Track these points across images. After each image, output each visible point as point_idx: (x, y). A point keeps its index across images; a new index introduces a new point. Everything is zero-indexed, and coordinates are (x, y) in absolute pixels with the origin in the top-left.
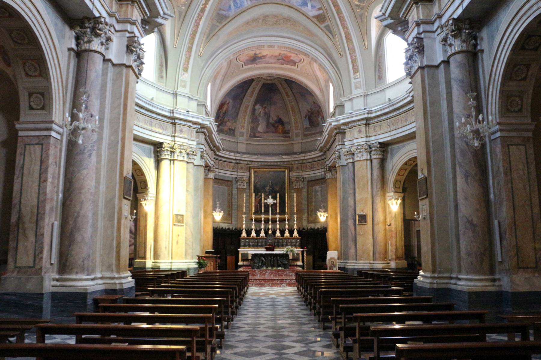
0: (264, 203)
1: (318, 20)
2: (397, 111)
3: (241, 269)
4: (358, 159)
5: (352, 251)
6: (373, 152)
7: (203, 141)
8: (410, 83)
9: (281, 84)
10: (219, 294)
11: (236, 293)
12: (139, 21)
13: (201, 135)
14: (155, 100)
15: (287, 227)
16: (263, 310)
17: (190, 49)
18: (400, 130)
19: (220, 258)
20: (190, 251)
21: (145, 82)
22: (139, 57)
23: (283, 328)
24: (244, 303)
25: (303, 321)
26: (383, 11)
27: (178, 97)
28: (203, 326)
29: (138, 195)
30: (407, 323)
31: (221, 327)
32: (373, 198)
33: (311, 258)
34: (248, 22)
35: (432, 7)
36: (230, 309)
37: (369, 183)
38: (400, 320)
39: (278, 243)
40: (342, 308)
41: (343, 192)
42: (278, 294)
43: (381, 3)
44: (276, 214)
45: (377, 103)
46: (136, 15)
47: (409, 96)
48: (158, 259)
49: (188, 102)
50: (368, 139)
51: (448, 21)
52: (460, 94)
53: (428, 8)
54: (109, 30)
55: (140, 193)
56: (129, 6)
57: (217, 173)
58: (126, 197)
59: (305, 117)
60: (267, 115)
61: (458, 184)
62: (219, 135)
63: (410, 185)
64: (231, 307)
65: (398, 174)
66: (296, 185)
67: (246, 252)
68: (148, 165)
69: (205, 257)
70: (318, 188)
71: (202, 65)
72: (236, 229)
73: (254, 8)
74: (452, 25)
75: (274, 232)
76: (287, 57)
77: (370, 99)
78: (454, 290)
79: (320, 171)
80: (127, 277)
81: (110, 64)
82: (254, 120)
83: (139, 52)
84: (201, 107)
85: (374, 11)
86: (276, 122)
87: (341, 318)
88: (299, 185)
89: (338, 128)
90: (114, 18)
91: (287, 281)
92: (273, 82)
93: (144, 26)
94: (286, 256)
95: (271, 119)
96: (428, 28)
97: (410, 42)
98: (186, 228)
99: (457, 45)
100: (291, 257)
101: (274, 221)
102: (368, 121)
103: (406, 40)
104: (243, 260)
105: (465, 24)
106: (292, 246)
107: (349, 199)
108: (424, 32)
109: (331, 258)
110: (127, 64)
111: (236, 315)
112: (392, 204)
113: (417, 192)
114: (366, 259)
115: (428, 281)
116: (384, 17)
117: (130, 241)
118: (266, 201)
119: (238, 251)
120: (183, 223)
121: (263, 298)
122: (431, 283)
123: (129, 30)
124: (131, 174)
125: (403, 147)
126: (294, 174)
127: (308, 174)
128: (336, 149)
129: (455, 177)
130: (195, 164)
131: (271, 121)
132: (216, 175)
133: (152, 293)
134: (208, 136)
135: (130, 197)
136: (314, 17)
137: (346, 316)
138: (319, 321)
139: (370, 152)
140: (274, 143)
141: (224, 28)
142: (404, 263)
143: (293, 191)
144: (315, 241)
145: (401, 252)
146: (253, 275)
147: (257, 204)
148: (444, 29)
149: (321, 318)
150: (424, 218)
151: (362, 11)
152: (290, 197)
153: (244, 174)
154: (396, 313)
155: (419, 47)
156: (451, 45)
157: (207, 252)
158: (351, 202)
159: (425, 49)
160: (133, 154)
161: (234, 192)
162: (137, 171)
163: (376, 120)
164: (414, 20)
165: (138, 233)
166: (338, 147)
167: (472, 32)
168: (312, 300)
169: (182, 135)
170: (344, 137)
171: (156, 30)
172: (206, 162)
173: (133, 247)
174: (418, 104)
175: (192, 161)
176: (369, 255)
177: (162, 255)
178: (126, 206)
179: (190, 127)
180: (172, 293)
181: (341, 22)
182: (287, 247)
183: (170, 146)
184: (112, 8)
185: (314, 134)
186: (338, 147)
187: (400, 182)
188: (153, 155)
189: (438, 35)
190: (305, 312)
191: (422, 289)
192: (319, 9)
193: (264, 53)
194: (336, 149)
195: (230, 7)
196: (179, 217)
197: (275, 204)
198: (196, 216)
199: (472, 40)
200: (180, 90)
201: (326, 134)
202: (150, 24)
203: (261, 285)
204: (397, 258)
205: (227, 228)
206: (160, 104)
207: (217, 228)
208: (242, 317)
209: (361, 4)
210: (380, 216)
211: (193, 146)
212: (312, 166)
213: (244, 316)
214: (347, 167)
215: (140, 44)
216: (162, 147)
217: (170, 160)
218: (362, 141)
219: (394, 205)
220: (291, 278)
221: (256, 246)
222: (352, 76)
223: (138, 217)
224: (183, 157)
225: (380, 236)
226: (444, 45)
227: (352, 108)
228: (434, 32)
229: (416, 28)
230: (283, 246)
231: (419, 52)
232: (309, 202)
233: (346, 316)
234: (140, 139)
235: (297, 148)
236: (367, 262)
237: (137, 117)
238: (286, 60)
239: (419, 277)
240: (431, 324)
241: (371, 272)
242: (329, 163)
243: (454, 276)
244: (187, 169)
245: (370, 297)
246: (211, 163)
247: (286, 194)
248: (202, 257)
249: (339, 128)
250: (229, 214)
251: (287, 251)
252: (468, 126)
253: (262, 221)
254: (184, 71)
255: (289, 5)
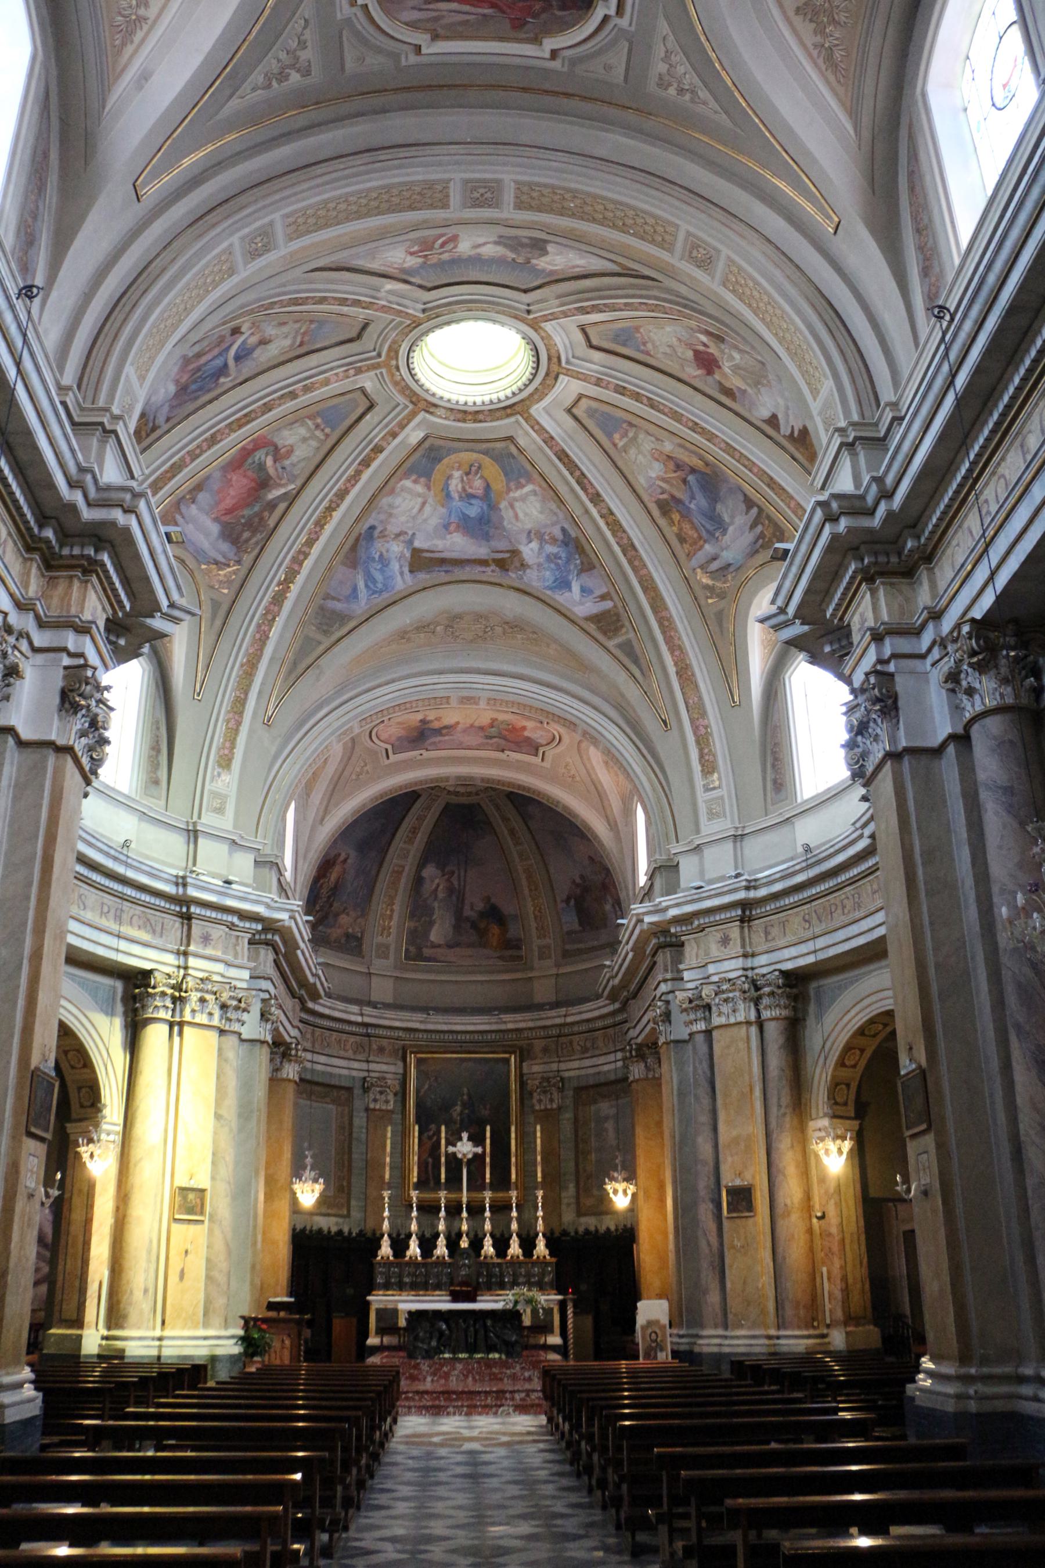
0: (447, 1155)
1: (599, 628)
2: (827, 881)
3: (374, 1360)
4: (723, 1020)
5: (713, 1298)
6: (766, 1001)
7: (270, 970)
8: (865, 799)
9: (498, 807)
10: (302, 1438)
11: (359, 1438)
12: (101, 624)
13: (262, 952)
14: (133, 846)
15: (514, 1226)
16: (441, 1491)
17: (239, 705)
18: (841, 935)
19: (310, 1324)
20: (220, 1302)
21: (110, 795)
22: (95, 725)
23: (505, 1551)
24: (385, 1470)
25: (570, 1526)
26: (780, 602)
27: (201, 841)
28: (255, 1547)
29: (70, 1127)
30: (896, 1530)
31: (309, 1552)
32: (768, 1135)
33: (588, 1321)
34: (406, 632)
35: (914, 590)
36: (339, 1488)
37: (758, 1092)
38: (870, 1519)
39: (490, 1275)
40: (689, 1481)
41: (680, 1121)
42: (488, 1439)
43: (772, 581)
44: (482, 1188)
45: (771, 860)
46: (93, 608)
47: (861, 836)
48: (120, 1326)
49: (230, 853)
50: (749, 963)
51: (958, 626)
52: (1004, 827)
53: (900, 592)
54: (15, 647)
55: (80, 1120)
56: (76, 584)
57: (309, 1065)
58: (33, 1130)
59: (567, 901)
60: (457, 896)
61: (1019, 1088)
62: (315, 951)
63: (877, 1097)
64: (342, 1481)
65: (841, 1063)
66: (540, 1101)
67: (390, 1306)
68: (104, 1037)
69: (264, 1320)
70: (605, 1107)
71: (273, 750)
72: (361, 1233)
73: (423, 594)
74: (970, 638)
75: (477, 1244)
76: (514, 729)
77: (753, 848)
78: (1031, 1418)
79: (611, 1057)
80: (19, 1385)
81: (11, 741)
82: (419, 909)
83: (95, 710)
84: (265, 871)
85: (755, 602)
86: (482, 915)
87: (686, 1516)
88: (551, 1100)
89: (661, 930)
90: (31, 615)
91: (517, 1396)
92: (473, 799)
93: (113, 638)
94: (511, 1316)
95: (467, 907)
96: (904, 645)
97: (857, 684)
98: (211, 1231)
99: (988, 690)
100: (527, 1321)
101: (476, 1211)
102: (746, 912)
103: (848, 680)
104: (381, 1331)
105: (1005, 635)
106: (530, 1285)
107: (700, 1140)
108: (894, 656)
109: (650, 1323)
110: (61, 742)
111: (358, 1508)
112: (827, 1152)
113: (898, 1113)
114: (754, 1325)
115: (950, 1389)
116: (782, 618)
117: (37, 1270)
118: (451, 1149)
119: (368, 1304)
120: (202, 1213)
121: (443, 1452)
122: (958, 1397)
123: (71, 647)
124: (51, 1063)
125: (852, 983)
126: (536, 1069)
127: (576, 1068)
128: (658, 993)
129: (1007, 1066)
130: (244, 1036)
131: (467, 912)
132: (304, 1069)
133: (94, 1438)
134: (285, 956)
135: (47, 1130)
136: (590, 619)
137: (704, 1509)
138: (618, 1527)
139: (757, 1001)
140: (476, 976)
141: (336, 649)
142: (870, 1335)
143: (531, 1119)
144: (599, 1267)
145: (860, 1299)
146: (413, 1378)
147: (425, 1156)
148: (950, 648)
149: (623, 1515)
150: (925, 1193)
151: (723, 604)
152: (526, 1138)
153: (386, 1068)
154: (858, 1497)
155: (880, 701)
156: (970, 692)
157: (271, 1306)
158: (705, 1149)
159: (900, 703)
160: (63, 1002)
161: (356, 1122)
162: (71, 1055)
163: (771, 906)
164: (867, 624)
165: (63, 1242)
166: (663, 988)
167: (1026, 656)
168: (595, 1457)
169: (209, 951)
170: (678, 959)
171: (146, 649)
172: (276, 1030)
173: (44, 1288)
174: (890, 857)
175: (236, 1027)
176: (763, 1312)
177: (133, 1316)
178: (33, 1158)
179: (231, 927)
180: (158, 1437)
181: (664, 633)
182: (516, 1290)
183: (174, 982)
184: (26, 586)
185: (594, 949)
186: (663, 988)
187: (848, 1085)
188: (120, 1008)
189: (933, 665)
190: (574, 1498)
191: (931, 1417)
192: (603, 597)
193: (449, 718)
194: (658, 993)
195: (355, 589)
196: (191, 1196)
197: (478, 1159)
198: (241, 1192)
199: (1027, 677)
200: (208, 820)
201: (626, 949)
202: (131, 632)
203: (436, 1411)
204: (849, 1319)
205: (334, 1229)
206: (148, 857)
207: (304, 1230)
208: (376, 1517)
209: (718, 584)
210: (791, 1190)
211: (239, 985)
212: (589, 1044)
213: (383, 1513)
214: (690, 1047)
215: (99, 688)
216: (149, 986)
217: (171, 1025)
218: (732, 967)
219: (834, 1158)
220: (527, 1386)
221: (420, 1285)
222: (699, 781)
223: (67, 1196)
224: (210, 1014)
225: (796, 1253)
226: (953, 691)
227: (702, 872)
228: (923, 657)
229: (873, 648)
230: (502, 1286)
231: (884, 713)
232: (580, 1153)
233: (704, 1509)
234: (84, 958)
235: (543, 991)
236: (757, 1333)
237: (80, 896)
238: (510, 738)
239: (921, 1376)
240: (971, 1532)
241: (774, 1364)
242: (638, 1034)
243: (1028, 1371)
244: (220, 1049)
245: (774, 1445)
246: (290, 1033)
247: (513, 1128)
248: (256, 1319)
249: (666, 932)
250: (340, 1189)
251: (516, 1302)
252: (1035, 915)
253: (439, 1210)
254: (220, 765)
255: (521, 587)
